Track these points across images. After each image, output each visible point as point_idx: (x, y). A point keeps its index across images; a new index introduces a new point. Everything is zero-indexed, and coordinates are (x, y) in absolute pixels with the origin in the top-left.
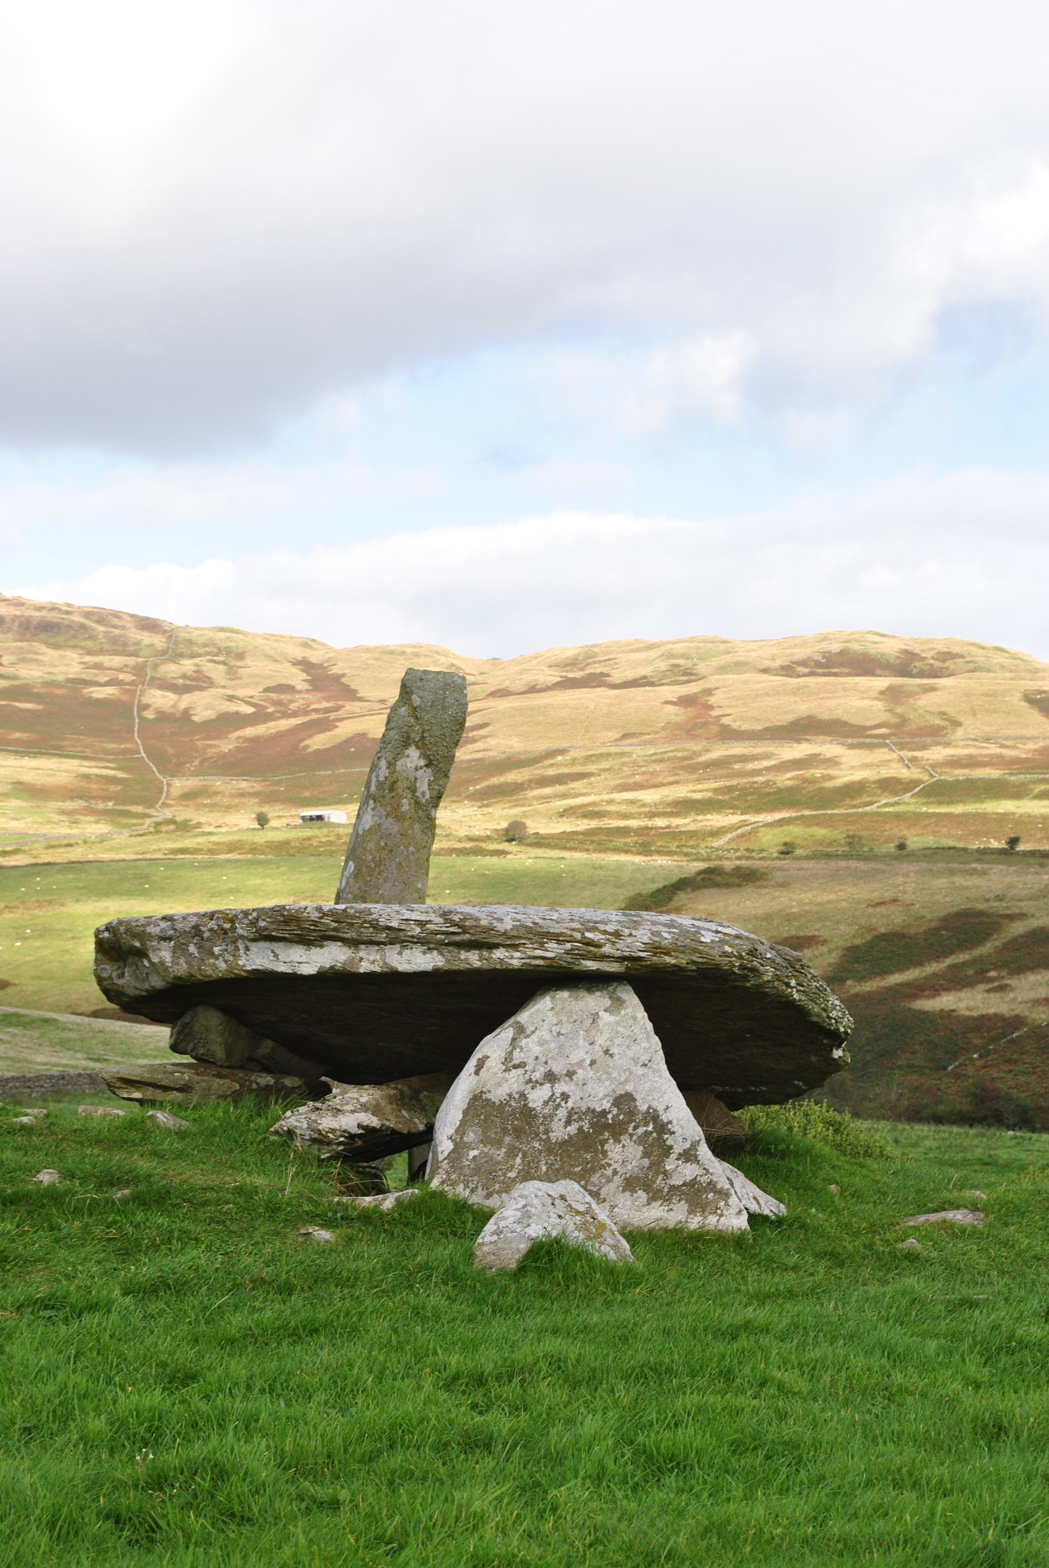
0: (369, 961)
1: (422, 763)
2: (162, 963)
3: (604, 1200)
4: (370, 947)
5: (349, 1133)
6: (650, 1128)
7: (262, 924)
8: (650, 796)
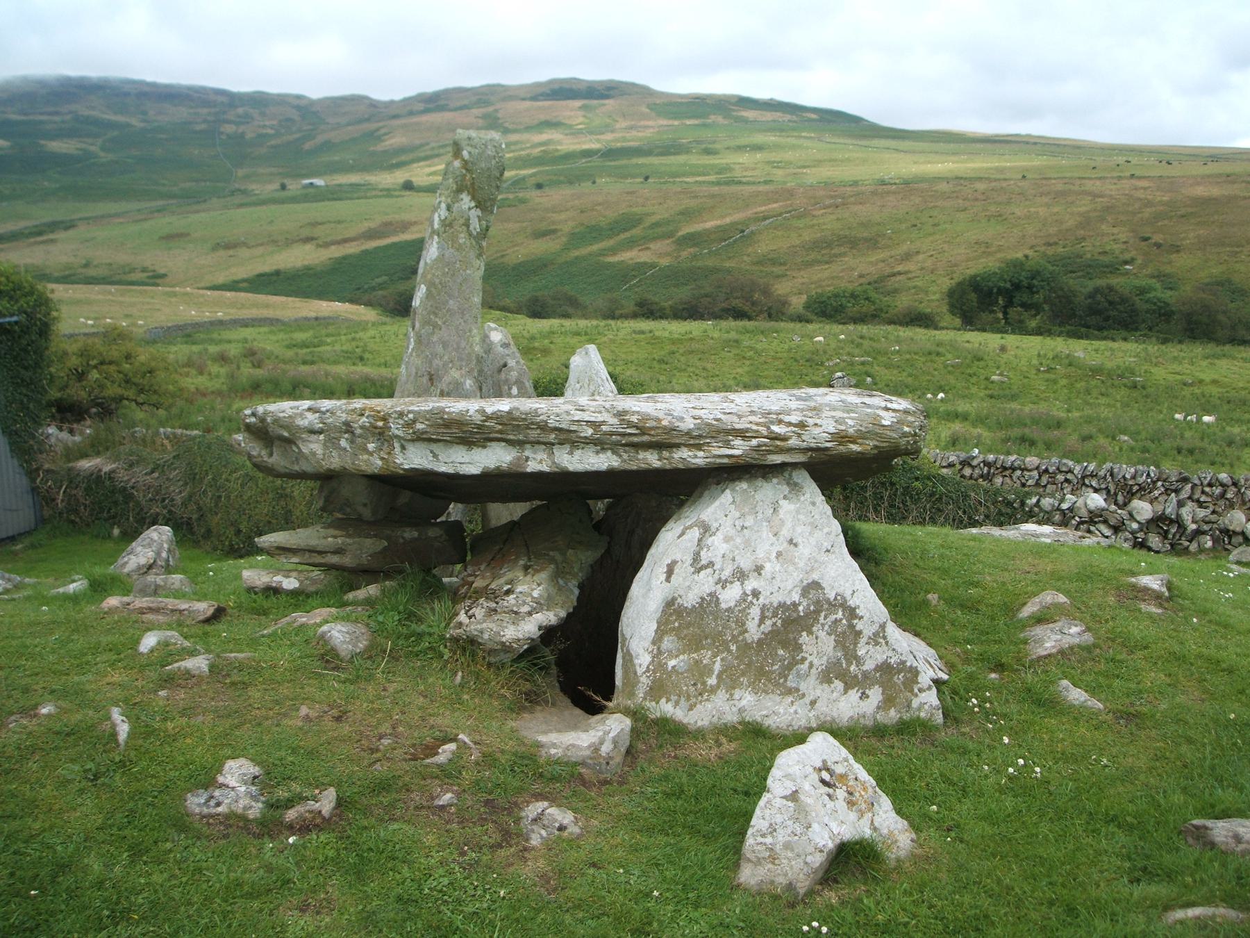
0: (537, 462)
1: (473, 204)
4: (537, 446)
7: (419, 426)
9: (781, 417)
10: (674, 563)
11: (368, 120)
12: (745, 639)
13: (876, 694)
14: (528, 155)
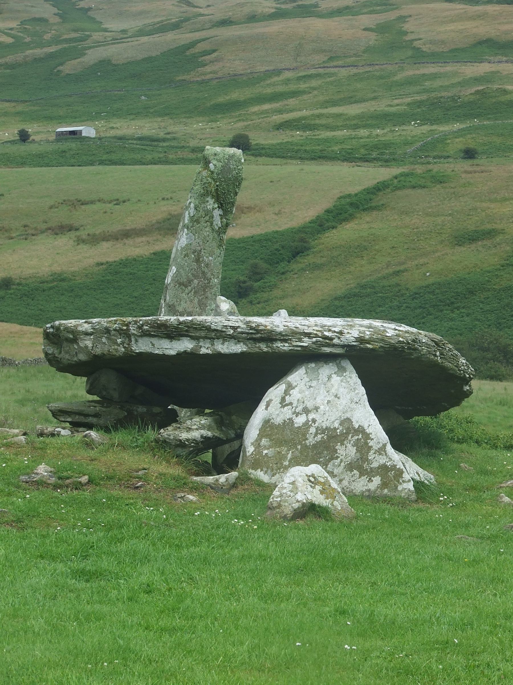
2: (87, 347)
3: (336, 476)
4: (206, 340)
5: (196, 441)
6: (360, 436)
8: (353, 110)
9: (330, 328)
10: (271, 400)
11: (176, 26)
12: (306, 443)
13: (377, 480)
14: (453, 99)
